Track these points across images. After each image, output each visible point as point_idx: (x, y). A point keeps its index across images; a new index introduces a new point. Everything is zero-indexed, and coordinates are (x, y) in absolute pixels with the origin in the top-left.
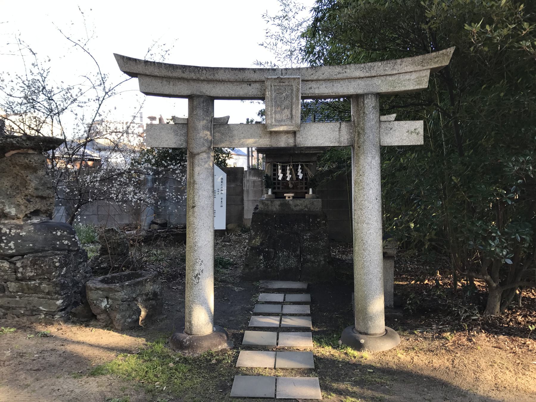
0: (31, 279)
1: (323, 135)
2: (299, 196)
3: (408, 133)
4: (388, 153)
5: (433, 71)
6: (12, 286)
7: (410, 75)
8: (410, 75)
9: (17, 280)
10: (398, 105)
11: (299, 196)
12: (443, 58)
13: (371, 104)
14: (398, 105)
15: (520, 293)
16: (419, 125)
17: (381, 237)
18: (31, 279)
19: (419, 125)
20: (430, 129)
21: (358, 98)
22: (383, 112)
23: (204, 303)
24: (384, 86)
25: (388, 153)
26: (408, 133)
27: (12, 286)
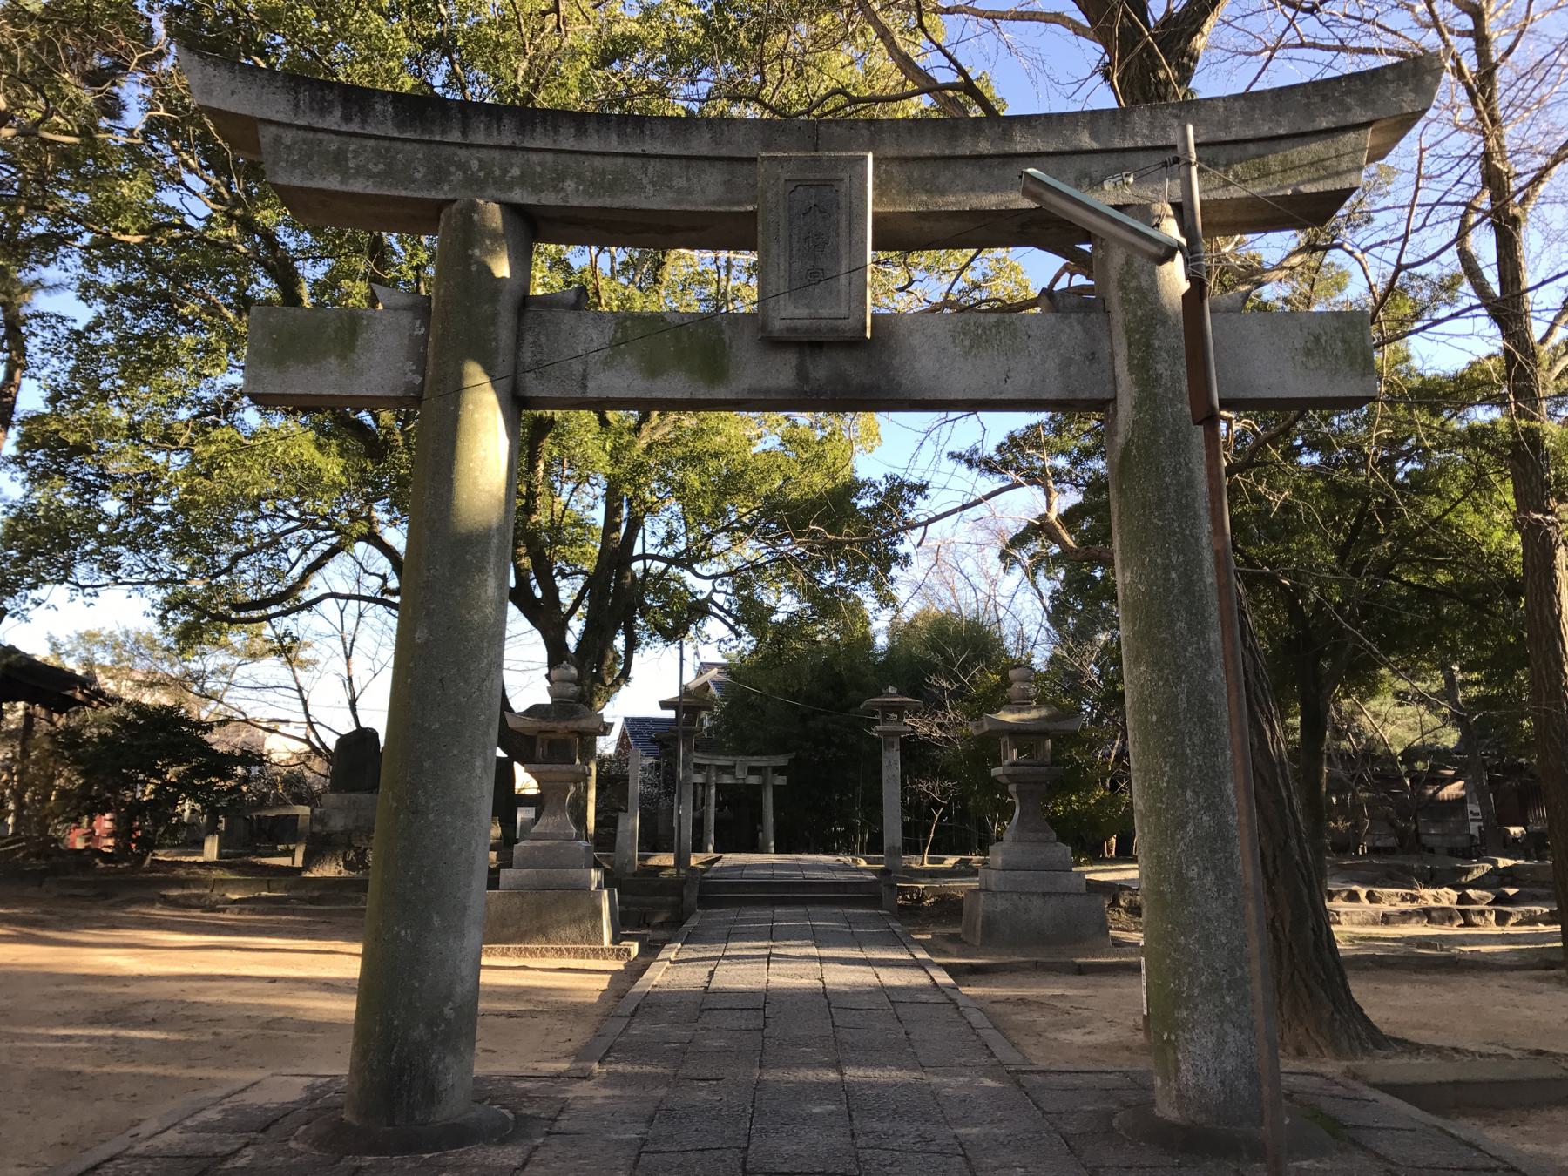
1: (753, 780)
3: (781, 780)
4: (776, 788)
7: (782, 761)
8: (782, 761)
10: (779, 770)
12: (792, 755)
14: (779, 770)
25: (776, 788)
26: (781, 780)
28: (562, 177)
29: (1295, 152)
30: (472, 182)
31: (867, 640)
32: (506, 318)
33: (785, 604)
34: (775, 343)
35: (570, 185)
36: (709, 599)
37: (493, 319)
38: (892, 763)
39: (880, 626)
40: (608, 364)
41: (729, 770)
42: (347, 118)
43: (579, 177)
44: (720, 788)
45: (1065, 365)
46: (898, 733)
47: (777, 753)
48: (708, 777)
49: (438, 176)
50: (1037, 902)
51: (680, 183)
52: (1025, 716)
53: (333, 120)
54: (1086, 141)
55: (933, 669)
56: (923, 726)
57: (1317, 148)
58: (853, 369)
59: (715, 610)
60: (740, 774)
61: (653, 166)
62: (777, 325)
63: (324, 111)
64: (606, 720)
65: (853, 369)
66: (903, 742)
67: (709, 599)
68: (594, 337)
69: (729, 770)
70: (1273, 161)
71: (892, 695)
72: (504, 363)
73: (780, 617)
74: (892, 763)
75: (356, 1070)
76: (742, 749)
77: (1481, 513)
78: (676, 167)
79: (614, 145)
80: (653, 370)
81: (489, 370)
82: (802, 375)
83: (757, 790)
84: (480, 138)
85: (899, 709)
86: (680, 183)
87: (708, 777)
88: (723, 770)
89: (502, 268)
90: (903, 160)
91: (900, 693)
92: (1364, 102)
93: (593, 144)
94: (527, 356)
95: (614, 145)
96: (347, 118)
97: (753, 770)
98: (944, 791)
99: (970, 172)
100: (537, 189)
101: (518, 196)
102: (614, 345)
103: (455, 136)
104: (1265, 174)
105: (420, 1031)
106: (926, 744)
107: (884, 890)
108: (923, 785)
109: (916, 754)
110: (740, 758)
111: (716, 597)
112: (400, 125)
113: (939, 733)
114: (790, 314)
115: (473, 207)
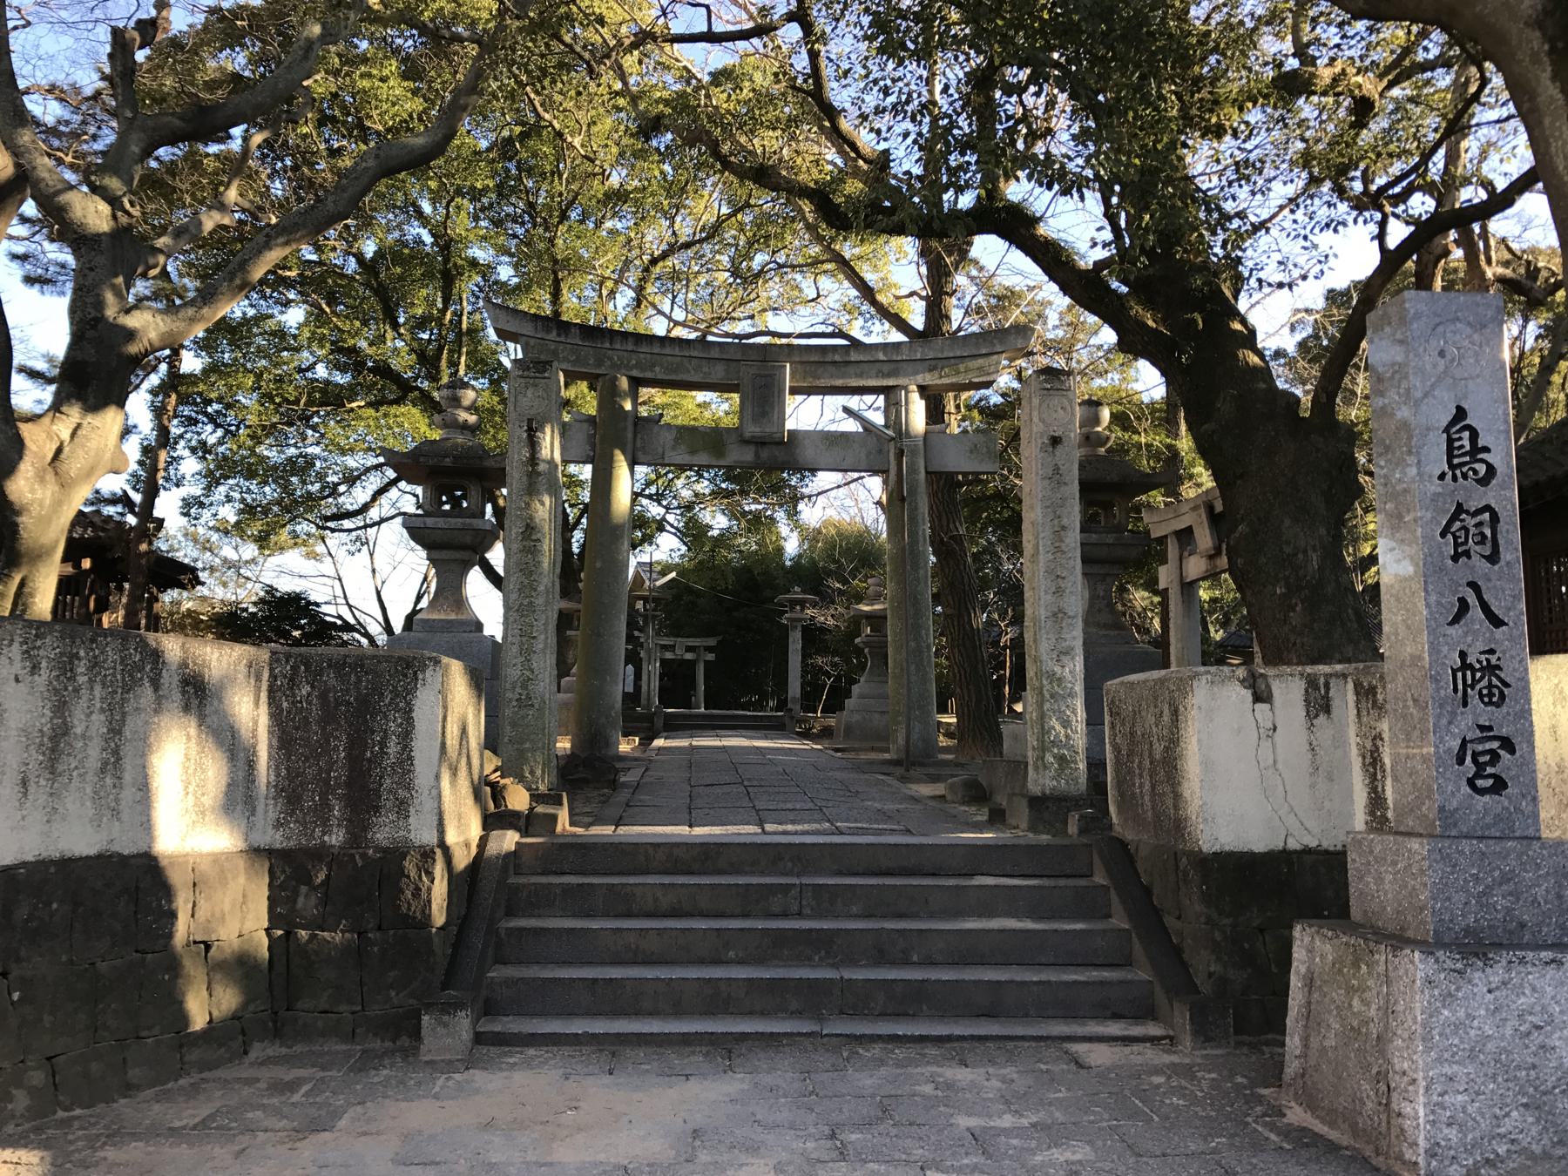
1: (689, 656)
3: (711, 657)
7: (712, 642)
8: (712, 642)
10: (709, 649)
14: (709, 649)
26: (711, 657)
28: (654, 365)
30: (614, 366)
31: (780, 551)
32: (630, 428)
33: (718, 522)
34: (746, 442)
35: (657, 369)
36: (664, 519)
37: (625, 429)
38: (795, 642)
39: (792, 546)
40: (673, 448)
41: (672, 648)
42: (559, 335)
43: (662, 366)
45: (868, 454)
46: (800, 620)
47: (708, 636)
49: (599, 363)
50: (877, 716)
51: (706, 369)
52: (876, 607)
53: (553, 336)
54: (881, 357)
55: (829, 573)
56: (825, 617)
57: (980, 361)
58: (779, 454)
59: (668, 528)
60: (678, 652)
61: (694, 362)
62: (747, 435)
63: (548, 331)
65: (779, 454)
66: (805, 629)
67: (664, 519)
68: (669, 437)
69: (672, 648)
70: (962, 367)
71: (797, 593)
72: (629, 447)
73: (715, 533)
74: (795, 642)
78: (704, 362)
79: (677, 352)
80: (693, 452)
81: (624, 453)
82: (757, 455)
83: (692, 664)
84: (618, 346)
85: (802, 603)
86: (706, 369)
89: (628, 406)
90: (802, 363)
91: (803, 592)
92: (1001, 342)
93: (667, 351)
94: (639, 444)
95: (677, 352)
96: (559, 335)
97: (689, 649)
98: (834, 665)
99: (831, 369)
100: (643, 370)
101: (635, 373)
102: (676, 440)
103: (607, 345)
104: (958, 373)
105: (603, 720)
106: (823, 630)
107: (787, 721)
108: (820, 661)
109: (814, 637)
111: (668, 517)
112: (583, 339)
113: (831, 622)
114: (752, 430)
115: (616, 378)
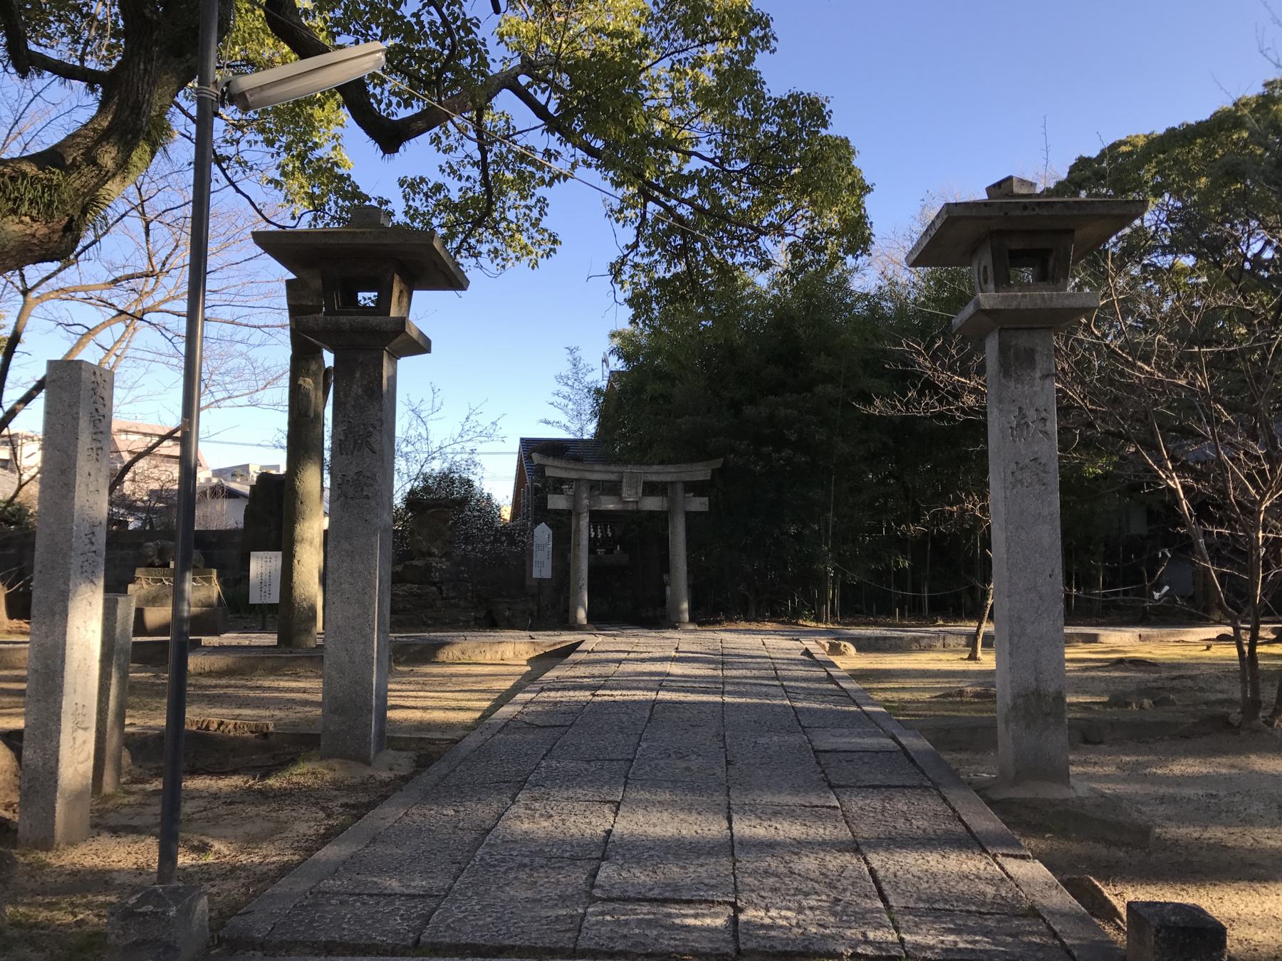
0: (453, 598)
1: (652, 504)
2: (610, 551)
3: (699, 504)
4: (688, 515)
5: (713, 470)
6: (439, 603)
7: (700, 472)
8: (700, 472)
9: (443, 599)
10: (695, 488)
11: (610, 551)
12: (718, 463)
13: (680, 487)
14: (695, 488)
15: (583, 132)
16: (706, 499)
17: (909, 246)
18: (453, 598)
19: (706, 499)
20: (1116, 594)
21: (672, 483)
22: (686, 492)
23: (583, 606)
24: (687, 478)
25: (688, 515)
26: (699, 504)
27: (439, 603)
29: (910, 860)
44: (598, 518)
47: (692, 460)
48: (575, 499)
60: (629, 495)
64: (630, 312)
69: (613, 489)
75: (1027, 266)
76: (642, 452)
77: (75, 166)
83: (661, 519)
87: (575, 499)
88: (597, 488)
97: (651, 489)
110: (628, 469)
